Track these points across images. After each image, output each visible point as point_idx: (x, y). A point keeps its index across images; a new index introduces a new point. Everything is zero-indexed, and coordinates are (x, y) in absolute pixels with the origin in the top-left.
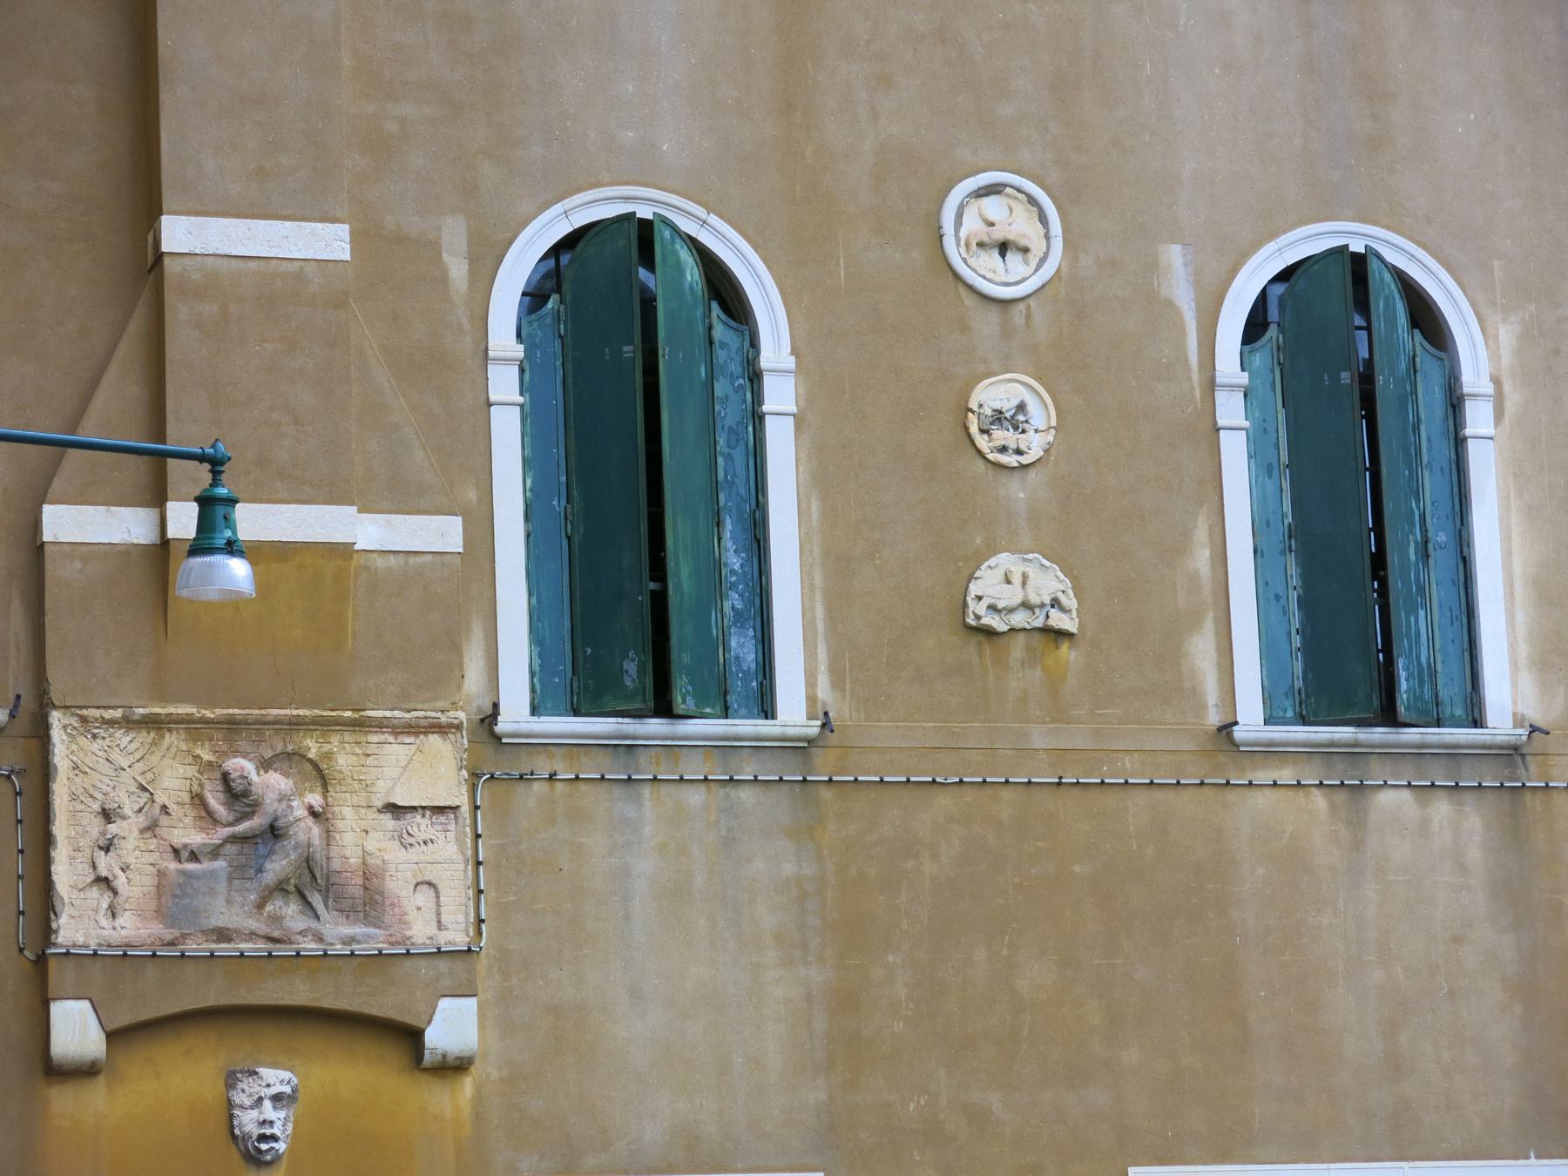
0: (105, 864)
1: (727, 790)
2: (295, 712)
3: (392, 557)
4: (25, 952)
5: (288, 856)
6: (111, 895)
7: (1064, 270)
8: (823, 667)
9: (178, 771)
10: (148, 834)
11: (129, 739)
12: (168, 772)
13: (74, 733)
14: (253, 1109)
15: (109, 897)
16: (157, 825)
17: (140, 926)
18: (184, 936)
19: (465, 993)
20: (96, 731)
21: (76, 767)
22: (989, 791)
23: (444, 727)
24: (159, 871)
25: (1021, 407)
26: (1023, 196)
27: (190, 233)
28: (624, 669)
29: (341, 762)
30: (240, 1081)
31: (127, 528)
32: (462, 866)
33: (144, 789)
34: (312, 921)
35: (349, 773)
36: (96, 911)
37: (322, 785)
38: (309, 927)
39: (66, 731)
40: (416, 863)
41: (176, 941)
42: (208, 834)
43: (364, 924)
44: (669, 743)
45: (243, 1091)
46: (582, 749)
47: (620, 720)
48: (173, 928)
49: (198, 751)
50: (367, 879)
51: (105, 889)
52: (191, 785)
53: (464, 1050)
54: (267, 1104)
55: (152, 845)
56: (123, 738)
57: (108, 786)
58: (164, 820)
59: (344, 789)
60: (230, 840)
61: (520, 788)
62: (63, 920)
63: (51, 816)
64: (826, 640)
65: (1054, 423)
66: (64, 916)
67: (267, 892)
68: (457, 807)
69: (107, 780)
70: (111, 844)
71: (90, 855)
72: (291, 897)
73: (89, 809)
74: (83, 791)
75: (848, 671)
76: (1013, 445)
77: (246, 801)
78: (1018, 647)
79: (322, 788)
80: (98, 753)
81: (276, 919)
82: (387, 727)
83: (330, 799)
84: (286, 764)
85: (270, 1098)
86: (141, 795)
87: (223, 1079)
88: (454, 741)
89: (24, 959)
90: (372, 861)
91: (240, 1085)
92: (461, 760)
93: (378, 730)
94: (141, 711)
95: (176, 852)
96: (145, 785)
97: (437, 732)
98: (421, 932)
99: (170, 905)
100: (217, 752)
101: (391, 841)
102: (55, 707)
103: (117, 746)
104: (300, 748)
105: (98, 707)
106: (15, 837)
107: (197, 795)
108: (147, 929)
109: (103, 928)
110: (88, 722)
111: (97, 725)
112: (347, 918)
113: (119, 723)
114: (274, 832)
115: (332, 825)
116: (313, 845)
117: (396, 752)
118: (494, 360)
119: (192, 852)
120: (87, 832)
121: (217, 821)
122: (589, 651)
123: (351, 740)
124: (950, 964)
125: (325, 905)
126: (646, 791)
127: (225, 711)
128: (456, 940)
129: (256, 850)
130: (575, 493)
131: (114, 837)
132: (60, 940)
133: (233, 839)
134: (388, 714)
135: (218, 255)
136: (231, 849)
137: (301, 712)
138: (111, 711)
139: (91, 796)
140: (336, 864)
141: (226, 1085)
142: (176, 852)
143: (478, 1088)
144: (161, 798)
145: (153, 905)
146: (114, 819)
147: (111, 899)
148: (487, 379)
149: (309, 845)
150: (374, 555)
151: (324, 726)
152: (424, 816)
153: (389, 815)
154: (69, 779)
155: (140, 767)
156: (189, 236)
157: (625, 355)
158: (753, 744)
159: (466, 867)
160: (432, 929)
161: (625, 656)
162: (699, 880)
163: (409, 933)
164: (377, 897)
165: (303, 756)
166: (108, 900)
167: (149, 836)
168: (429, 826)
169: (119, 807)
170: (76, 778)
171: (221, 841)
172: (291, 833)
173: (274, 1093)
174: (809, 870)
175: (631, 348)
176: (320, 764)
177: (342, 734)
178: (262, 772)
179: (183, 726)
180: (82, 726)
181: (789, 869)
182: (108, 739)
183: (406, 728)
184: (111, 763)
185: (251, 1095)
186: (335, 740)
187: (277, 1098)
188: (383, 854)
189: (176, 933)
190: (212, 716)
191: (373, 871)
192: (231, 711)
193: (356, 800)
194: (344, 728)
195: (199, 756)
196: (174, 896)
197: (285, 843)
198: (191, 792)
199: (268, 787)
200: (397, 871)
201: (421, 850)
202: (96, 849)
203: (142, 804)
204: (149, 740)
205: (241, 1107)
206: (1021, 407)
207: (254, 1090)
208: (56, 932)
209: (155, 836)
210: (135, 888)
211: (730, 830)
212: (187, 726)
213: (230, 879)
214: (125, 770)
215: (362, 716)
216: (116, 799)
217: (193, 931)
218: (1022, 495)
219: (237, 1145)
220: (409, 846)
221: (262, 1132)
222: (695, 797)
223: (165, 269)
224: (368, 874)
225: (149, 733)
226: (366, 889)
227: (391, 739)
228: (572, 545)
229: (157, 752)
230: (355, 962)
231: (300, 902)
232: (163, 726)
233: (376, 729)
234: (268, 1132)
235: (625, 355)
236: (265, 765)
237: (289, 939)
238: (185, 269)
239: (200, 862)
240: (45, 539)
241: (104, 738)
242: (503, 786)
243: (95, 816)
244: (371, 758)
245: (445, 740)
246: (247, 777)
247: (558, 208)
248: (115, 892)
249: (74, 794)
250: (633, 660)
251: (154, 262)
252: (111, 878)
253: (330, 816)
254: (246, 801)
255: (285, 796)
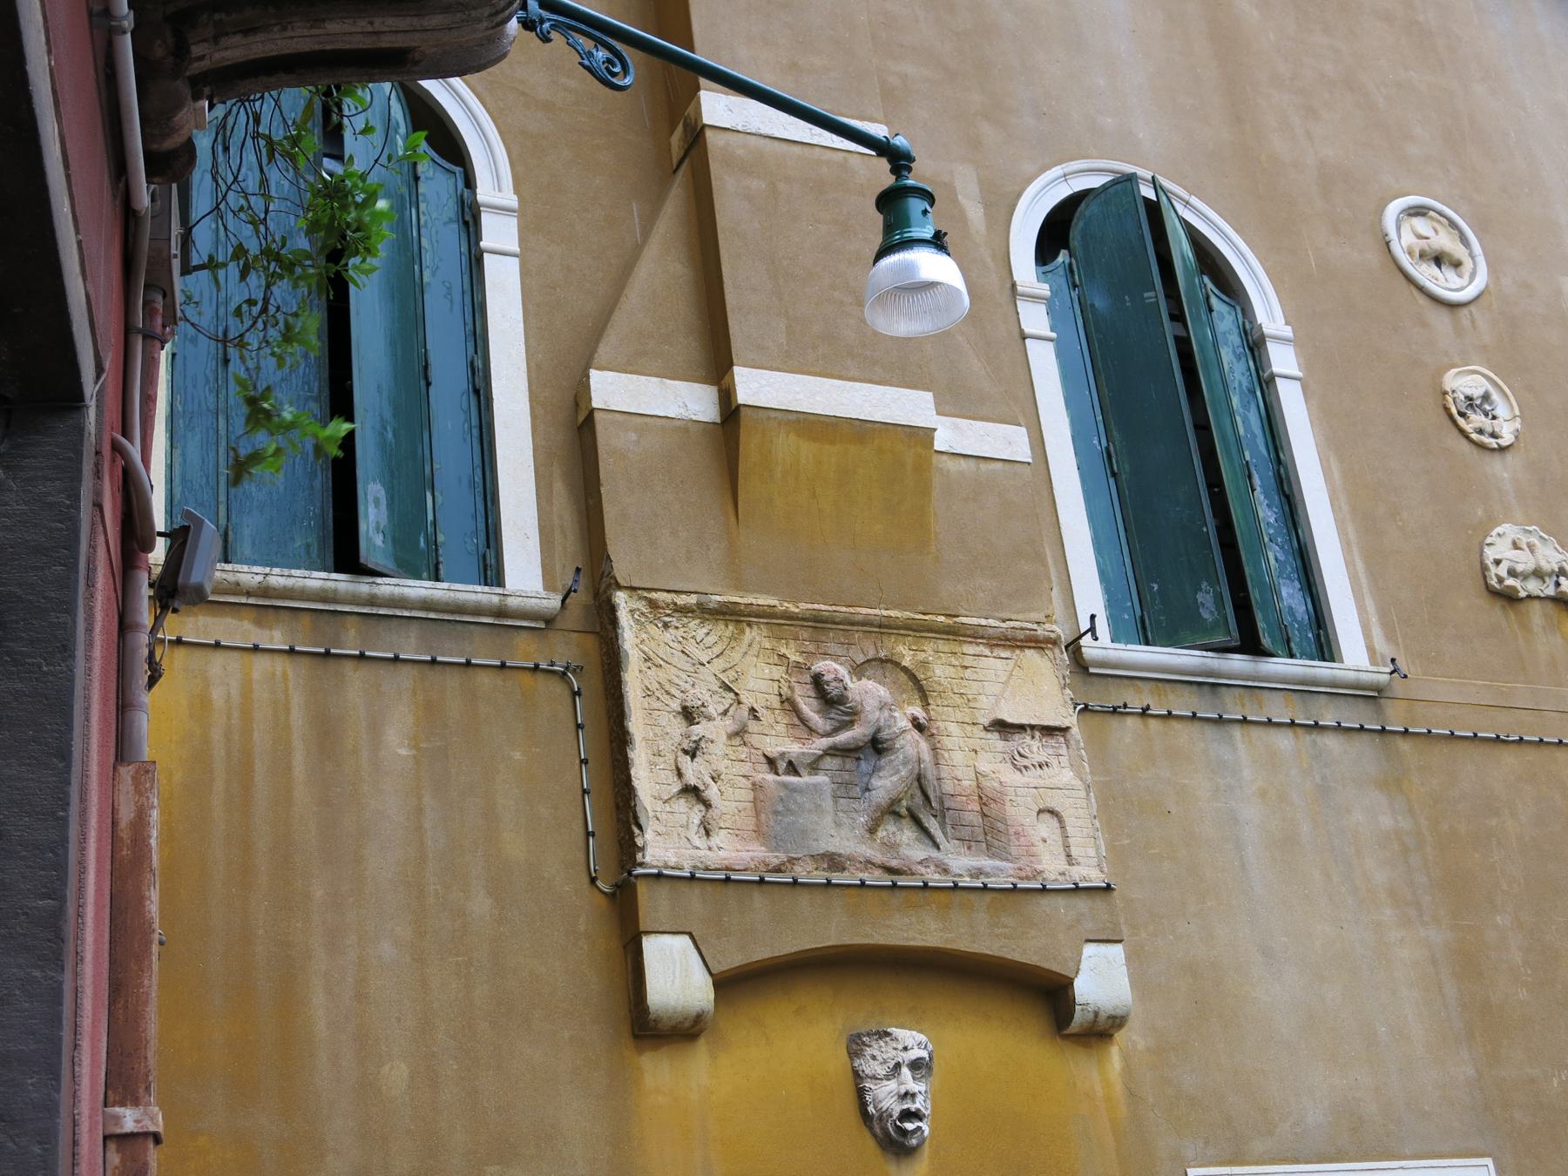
0: (694, 772)
1: (1313, 736)
2: (885, 613)
3: (962, 461)
4: (599, 883)
5: (898, 772)
6: (703, 808)
7: (1491, 286)
8: (1374, 620)
9: (763, 670)
10: (737, 741)
11: (705, 630)
12: (753, 671)
13: (643, 620)
14: (889, 1080)
15: (700, 811)
16: (746, 731)
17: (739, 848)
18: (792, 861)
19: (1110, 938)
20: (667, 619)
21: (647, 659)
22: (1546, 751)
23: (1041, 642)
24: (754, 784)
25: (1486, 397)
26: (1445, 220)
27: (730, 110)
28: (1199, 601)
29: (938, 672)
30: (866, 1045)
31: (684, 403)
32: (1083, 794)
33: (730, 689)
34: (931, 850)
35: (949, 686)
36: (687, 827)
37: (920, 697)
38: (930, 857)
39: (633, 615)
40: (1036, 788)
41: (783, 868)
42: (804, 744)
43: (988, 856)
44: (1250, 683)
45: (874, 1058)
46: (1167, 686)
47: (1204, 653)
48: (779, 851)
49: (783, 650)
50: (984, 804)
51: (694, 802)
52: (780, 687)
53: (1117, 1007)
54: (905, 1071)
55: (743, 752)
56: (694, 626)
57: (686, 682)
58: (753, 726)
59: (946, 703)
60: (831, 752)
61: (1114, 722)
62: (649, 835)
63: (626, 710)
64: (1371, 592)
65: (1517, 413)
66: (649, 831)
67: (879, 814)
68: (1067, 729)
69: (684, 676)
70: (697, 748)
71: (672, 761)
72: (904, 822)
73: (668, 709)
74: (658, 686)
75: (1397, 626)
76: (1489, 430)
77: (842, 708)
78: (1536, 612)
79: (921, 701)
80: (671, 644)
81: (891, 846)
82: (982, 638)
83: (932, 712)
84: (880, 672)
85: (908, 1065)
86: (725, 695)
87: (844, 1046)
88: (1052, 658)
89: (597, 892)
90: (988, 784)
91: (869, 1051)
92: (1064, 678)
93: (973, 640)
94: (718, 598)
95: (771, 762)
96: (729, 684)
97: (1034, 648)
98: (1052, 867)
99: (772, 823)
100: (803, 652)
101: (1003, 764)
102: (619, 587)
103: (692, 638)
104: (892, 654)
105: (669, 591)
106: (576, 746)
107: (787, 699)
108: (748, 851)
109: (698, 848)
110: (659, 607)
111: (668, 612)
112: (969, 848)
113: (693, 611)
114: (877, 746)
115: (939, 742)
116: (924, 761)
117: (993, 667)
118: (1022, 295)
119: (790, 763)
120: (667, 734)
121: (814, 731)
122: (1156, 587)
123: (946, 649)
124: (1553, 927)
125: (943, 833)
126: (1237, 732)
127: (810, 606)
128: (1091, 876)
129: (858, 767)
130: (1115, 433)
131: (700, 739)
132: (648, 859)
133: (834, 751)
134: (983, 622)
135: (761, 135)
136: (831, 763)
137: (892, 613)
138: (683, 596)
139: (668, 693)
140: (948, 787)
141: (849, 1053)
142: (771, 762)
143: (1126, 1058)
144: (748, 700)
145: (751, 823)
146: (697, 720)
147: (703, 814)
148: (1018, 313)
149: (919, 761)
150: (945, 457)
151: (918, 630)
152: (1033, 737)
153: (996, 735)
154: (640, 671)
155: (719, 664)
156: (730, 113)
157: (1147, 301)
158: (1329, 690)
159: (1088, 795)
160: (1062, 864)
161: (1198, 589)
162: (1305, 828)
163: (1039, 868)
164: (999, 824)
165: (897, 664)
166: (700, 815)
167: (738, 744)
168: (1041, 749)
169: (703, 705)
170: (649, 672)
171: (821, 752)
172: (897, 746)
173: (914, 1057)
174: (1405, 824)
175: (1152, 294)
176: (917, 674)
177: (935, 643)
178: (855, 679)
179: (765, 621)
180: (651, 613)
181: (1386, 822)
182: (683, 629)
183: (1002, 640)
184: (688, 656)
185: (885, 1062)
186: (929, 647)
187: (916, 1065)
188: (997, 775)
189: (783, 857)
190: (797, 610)
191: (991, 796)
192: (816, 606)
193: (959, 716)
194: (938, 636)
195: (784, 656)
196: (776, 813)
197: (892, 757)
198: (780, 695)
199: (866, 692)
200: (1016, 795)
201: (1038, 773)
202: (680, 753)
203: (727, 706)
204: (728, 633)
205: (874, 1077)
206: (1486, 397)
207: (889, 1055)
208: (642, 849)
209: (745, 744)
210: (729, 800)
211: (1324, 778)
212: (769, 621)
213: (836, 798)
214: (704, 665)
215: (955, 622)
216: (700, 696)
217: (800, 855)
218: (1505, 475)
219: (871, 1129)
220: (1024, 770)
221: (905, 1107)
222: (1284, 741)
223: (708, 141)
224: (985, 799)
225: (727, 626)
226: (984, 815)
227: (987, 652)
228: (1119, 483)
229: (737, 648)
230: (988, 897)
231: (914, 828)
232: (742, 619)
233: (970, 639)
234: (913, 1107)
235: (1147, 301)
236: (858, 670)
237: (910, 869)
238: (728, 144)
239: (801, 776)
240: (595, 405)
241: (677, 628)
242: (1098, 719)
243: (674, 716)
244: (968, 670)
245: (1042, 657)
246: (842, 680)
247: (1057, 171)
248: (707, 805)
249: (648, 689)
250: (1208, 593)
251: (696, 134)
252: (702, 788)
253: (935, 731)
254: (842, 708)
255: (885, 704)
